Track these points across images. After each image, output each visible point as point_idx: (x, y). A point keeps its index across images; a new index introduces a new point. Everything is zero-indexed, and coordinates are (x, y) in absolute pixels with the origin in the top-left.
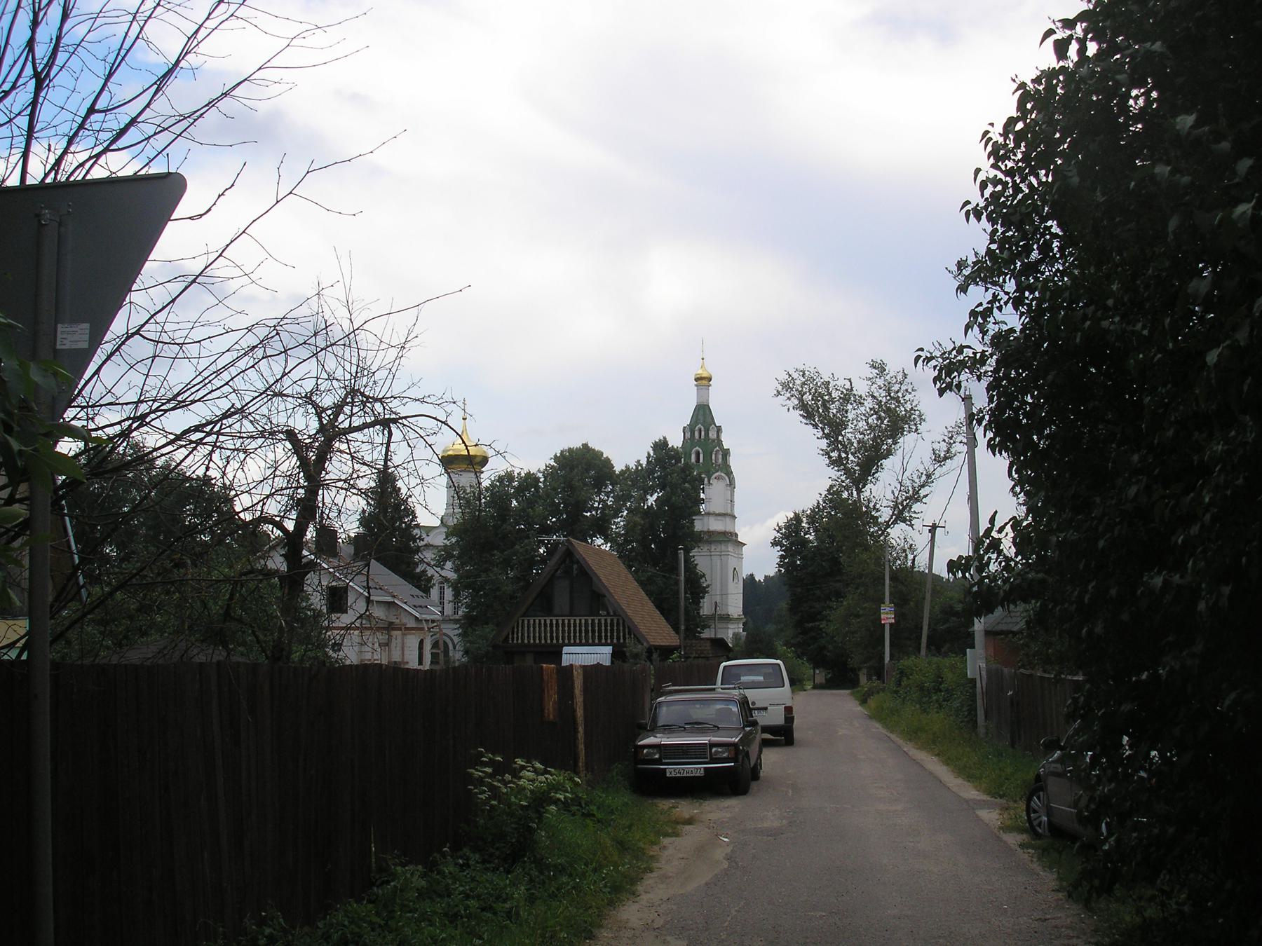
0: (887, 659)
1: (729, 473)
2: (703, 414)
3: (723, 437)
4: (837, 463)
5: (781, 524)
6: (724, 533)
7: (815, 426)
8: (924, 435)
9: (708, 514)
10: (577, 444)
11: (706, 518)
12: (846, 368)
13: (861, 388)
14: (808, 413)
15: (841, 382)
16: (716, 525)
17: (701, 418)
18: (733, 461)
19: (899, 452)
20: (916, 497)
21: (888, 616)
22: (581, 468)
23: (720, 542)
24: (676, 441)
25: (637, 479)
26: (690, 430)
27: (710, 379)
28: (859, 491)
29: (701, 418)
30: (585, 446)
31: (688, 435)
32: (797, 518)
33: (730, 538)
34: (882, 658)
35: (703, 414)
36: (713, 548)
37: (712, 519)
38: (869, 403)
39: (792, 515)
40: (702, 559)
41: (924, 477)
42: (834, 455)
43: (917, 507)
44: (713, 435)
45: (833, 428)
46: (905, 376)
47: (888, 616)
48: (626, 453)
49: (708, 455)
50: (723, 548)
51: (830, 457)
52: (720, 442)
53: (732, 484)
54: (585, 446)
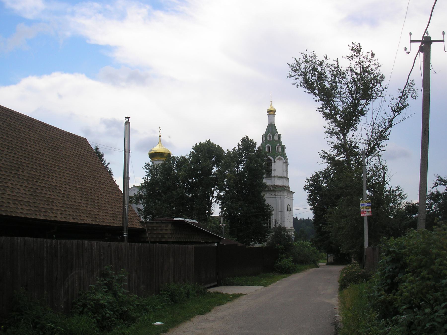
0: (366, 245)
1: (285, 156)
2: (271, 128)
3: (282, 139)
4: (328, 116)
5: (309, 178)
6: (283, 186)
7: (315, 94)
8: (386, 98)
9: (274, 177)
10: (204, 141)
11: (273, 179)
12: (335, 51)
13: (344, 65)
14: (310, 86)
15: (331, 62)
16: (278, 182)
17: (270, 130)
18: (287, 151)
19: (369, 114)
20: (382, 137)
21: (366, 210)
22: (207, 152)
23: (280, 191)
24: (258, 141)
25: (234, 157)
26: (265, 136)
27: (275, 111)
28: (344, 135)
29: (270, 130)
30: (209, 141)
31: (264, 139)
32: (317, 175)
33: (286, 189)
34: (363, 245)
35: (271, 128)
36: (277, 193)
37: (276, 179)
38: (349, 77)
39: (315, 174)
40: (269, 199)
41: (387, 124)
42: (327, 111)
43: (383, 143)
44: (276, 138)
45: (326, 95)
46: (373, 55)
47: (366, 210)
48: (229, 144)
49: (274, 148)
50: (282, 193)
51: (324, 113)
52: (280, 142)
53: (286, 162)
54: (209, 141)
